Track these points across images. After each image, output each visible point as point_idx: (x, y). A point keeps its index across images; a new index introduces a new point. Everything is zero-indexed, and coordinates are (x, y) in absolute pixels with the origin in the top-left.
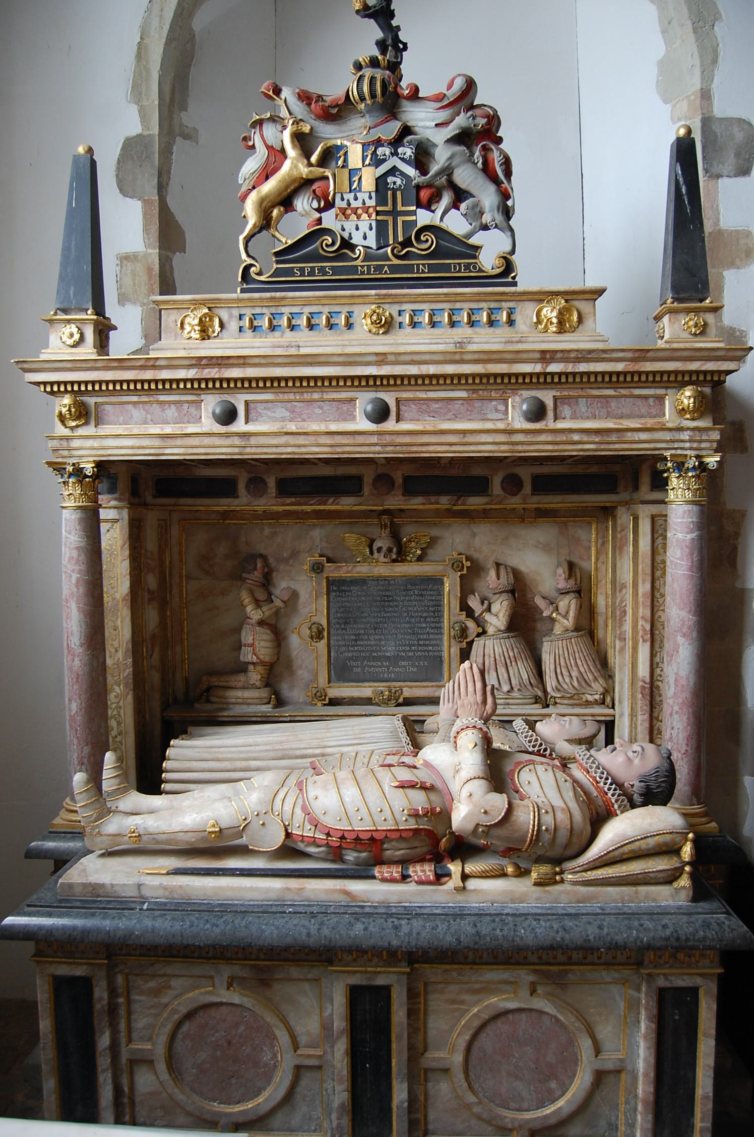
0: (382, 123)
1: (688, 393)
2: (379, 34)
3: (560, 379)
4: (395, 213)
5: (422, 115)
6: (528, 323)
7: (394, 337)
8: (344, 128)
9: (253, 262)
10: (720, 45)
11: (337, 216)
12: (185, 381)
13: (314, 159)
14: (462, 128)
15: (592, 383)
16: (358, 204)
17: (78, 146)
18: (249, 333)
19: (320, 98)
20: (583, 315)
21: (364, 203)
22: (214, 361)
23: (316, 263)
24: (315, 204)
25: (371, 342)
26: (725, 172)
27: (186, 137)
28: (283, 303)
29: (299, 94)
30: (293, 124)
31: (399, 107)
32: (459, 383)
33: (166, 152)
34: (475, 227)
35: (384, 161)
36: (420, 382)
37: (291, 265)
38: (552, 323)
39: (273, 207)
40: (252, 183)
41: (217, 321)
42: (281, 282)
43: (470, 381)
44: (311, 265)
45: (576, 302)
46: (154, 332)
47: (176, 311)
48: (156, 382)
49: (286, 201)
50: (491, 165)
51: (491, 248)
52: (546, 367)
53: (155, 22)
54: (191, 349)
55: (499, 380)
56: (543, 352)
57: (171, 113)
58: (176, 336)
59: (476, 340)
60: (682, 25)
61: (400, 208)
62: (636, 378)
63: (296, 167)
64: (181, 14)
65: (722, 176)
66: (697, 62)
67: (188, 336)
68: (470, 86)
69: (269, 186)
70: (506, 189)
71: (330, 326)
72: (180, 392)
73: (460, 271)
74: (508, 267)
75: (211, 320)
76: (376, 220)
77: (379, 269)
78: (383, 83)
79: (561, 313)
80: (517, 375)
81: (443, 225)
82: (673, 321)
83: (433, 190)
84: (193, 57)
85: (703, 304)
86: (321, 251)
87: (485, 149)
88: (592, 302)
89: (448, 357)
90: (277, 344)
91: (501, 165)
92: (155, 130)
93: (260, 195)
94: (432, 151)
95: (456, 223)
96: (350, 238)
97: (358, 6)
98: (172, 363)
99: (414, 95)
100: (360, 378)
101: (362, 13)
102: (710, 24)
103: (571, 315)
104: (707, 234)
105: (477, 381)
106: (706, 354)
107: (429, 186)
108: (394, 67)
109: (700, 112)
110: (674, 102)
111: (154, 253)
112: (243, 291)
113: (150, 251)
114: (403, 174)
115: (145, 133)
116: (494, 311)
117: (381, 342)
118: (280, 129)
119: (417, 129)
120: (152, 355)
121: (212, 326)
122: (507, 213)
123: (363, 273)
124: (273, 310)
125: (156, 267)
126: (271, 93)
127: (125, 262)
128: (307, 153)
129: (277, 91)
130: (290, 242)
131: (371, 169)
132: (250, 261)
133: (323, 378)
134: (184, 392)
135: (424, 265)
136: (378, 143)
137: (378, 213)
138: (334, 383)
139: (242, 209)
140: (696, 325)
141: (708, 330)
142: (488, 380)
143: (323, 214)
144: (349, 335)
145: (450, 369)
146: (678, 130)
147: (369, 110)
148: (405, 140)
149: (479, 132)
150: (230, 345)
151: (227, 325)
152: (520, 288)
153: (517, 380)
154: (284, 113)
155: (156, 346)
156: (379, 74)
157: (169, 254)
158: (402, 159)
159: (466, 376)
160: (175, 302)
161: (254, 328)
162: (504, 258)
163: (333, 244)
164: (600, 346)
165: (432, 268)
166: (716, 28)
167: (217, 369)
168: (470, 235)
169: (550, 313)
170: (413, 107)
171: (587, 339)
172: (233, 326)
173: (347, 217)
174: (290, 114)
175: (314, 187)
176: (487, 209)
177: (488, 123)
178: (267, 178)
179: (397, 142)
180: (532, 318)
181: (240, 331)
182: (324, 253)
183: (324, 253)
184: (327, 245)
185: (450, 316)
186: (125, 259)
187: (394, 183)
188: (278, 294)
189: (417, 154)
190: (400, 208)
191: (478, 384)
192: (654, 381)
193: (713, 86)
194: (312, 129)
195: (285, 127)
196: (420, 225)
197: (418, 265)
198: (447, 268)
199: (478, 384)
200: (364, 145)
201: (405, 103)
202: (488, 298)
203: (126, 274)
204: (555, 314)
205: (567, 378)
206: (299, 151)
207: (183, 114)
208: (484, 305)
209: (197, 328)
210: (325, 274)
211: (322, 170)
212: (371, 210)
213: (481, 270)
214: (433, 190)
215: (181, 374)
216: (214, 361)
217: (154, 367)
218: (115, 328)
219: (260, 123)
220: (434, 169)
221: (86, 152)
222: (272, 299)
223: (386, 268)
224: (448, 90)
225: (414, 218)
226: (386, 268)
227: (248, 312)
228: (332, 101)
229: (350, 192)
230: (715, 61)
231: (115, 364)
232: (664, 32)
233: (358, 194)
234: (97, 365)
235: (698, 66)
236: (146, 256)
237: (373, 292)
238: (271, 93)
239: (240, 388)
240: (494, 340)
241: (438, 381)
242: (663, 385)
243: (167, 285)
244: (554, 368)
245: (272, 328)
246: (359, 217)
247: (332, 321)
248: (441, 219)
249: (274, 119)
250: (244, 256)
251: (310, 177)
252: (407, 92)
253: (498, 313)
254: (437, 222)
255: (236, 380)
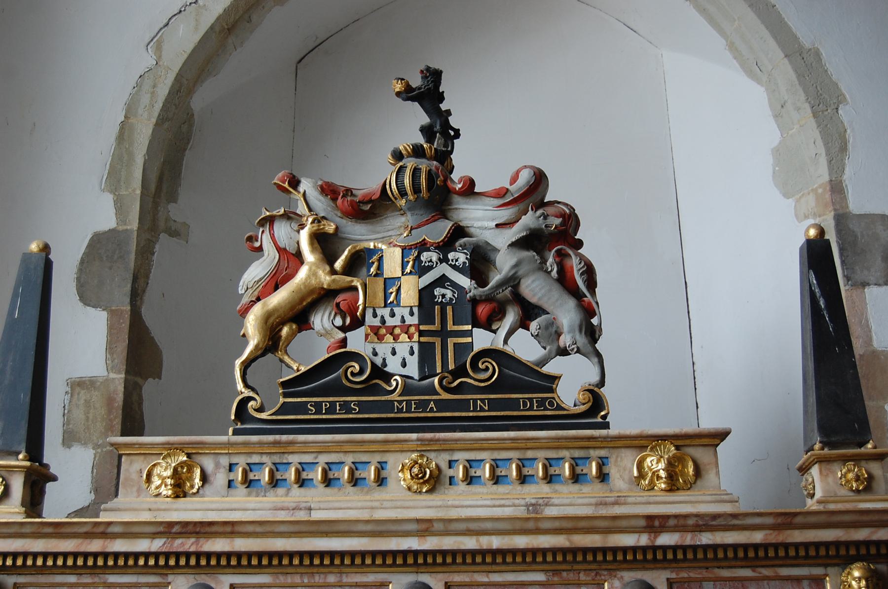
0: (428, 222)
1: (857, 574)
2: (424, 119)
3: (675, 555)
4: (444, 334)
5: (479, 214)
6: (626, 477)
7: (443, 497)
8: (378, 228)
9: (252, 394)
10: (848, 131)
11: (367, 336)
12: (147, 555)
13: (338, 264)
14: (530, 229)
15: (721, 560)
16: (396, 321)
17: (31, 242)
18: (242, 489)
19: (348, 192)
20: (702, 467)
21: (403, 320)
22: (190, 528)
23: (338, 399)
24: (339, 321)
25: (411, 504)
26: (872, 279)
27: (174, 233)
28: (290, 449)
29: (321, 187)
30: (313, 222)
31: (450, 204)
32: (534, 561)
33: (145, 252)
34: (550, 351)
35: (430, 268)
36: (479, 559)
37: (304, 399)
38: (659, 478)
39: (283, 323)
40: (256, 293)
41: (197, 473)
42: (291, 420)
43: (549, 558)
44: (331, 399)
45: (690, 451)
46: (108, 485)
47: (142, 458)
48: (106, 555)
49: (300, 316)
50: (569, 274)
51: (572, 378)
52: (655, 538)
53: (145, 99)
54: (159, 510)
55: (590, 557)
56: (650, 518)
57: (156, 204)
58: (139, 491)
59: (556, 501)
60: (798, 109)
61: (450, 327)
62: (781, 553)
63: (315, 274)
64: (179, 91)
65: (868, 284)
66: (822, 151)
67: (156, 492)
68: (540, 179)
69: (279, 298)
70: (590, 303)
71: (355, 481)
72: (139, 570)
73: (531, 408)
74: (596, 403)
75: (190, 470)
76: (419, 342)
77: (422, 405)
78: (431, 176)
79: (670, 465)
80: (615, 550)
81: (508, 349)
82: (824, 473)
83: (494, 305)
84: (189, 141)
85: (863, 450)
86: (344, 381)
87: (561, 255)
88: (712, 449)
89: (518, 525)
90: (280, 505)
91: (582, 274)
92: (134, 225)
93: (266, 309)
94: (492, 256)
95: (525, 347)
96: (385, 364)
97: (399, 87)
98: (130, 531)
99: (469, 189)
100: (394, 554)
101: (404, 95)
102: (833, 107)
103: (685, 466)
104: (857, 357)
105: (559, 558)
106: (876, 517)
107: (488, 299)
108: (444, 157)
109: (831, 208)
110: (797, 196)
111: (119, 378)
112: (236, 432)
113: (112, 375)
114: (454, 285)
115: (121, 228)
116: (579, 462)
117: (424, 503)
118: (296, 228)
119: (472, 230)
120: (104, 518)
121: (191, 479)
122: (592, 334)
123: (400, 411)
124: (277, 459)
125: (120, 397)
126: (286, 185)
127: (78, 389)
128: (329, 258)
129: (295, 183)
130: (303, 369)
131: (413, 278)
132: (247, 393)
133: (342, 554)
134: (145, 571)
135: (482, 400)
136: (423, 246)
137: (421, 333)
138: (358, 561)
139: (242, 325)
140: (857, 479)
141: (875, 485)
142: (575, 557)
143: (348, 334)
144: (380, 495)
145: (521, 542)
146: (807, 230)
147: (412, 207)
148: (457, 244)
149: (552, 234)
150: (213, 506)
151: (212, 479)
152: (613, 431)
153: (615, 556)
154: (302, 209)
155: (109, 505)
156: (424, 165)
157: (139, 380)
158: (454, 267)
159: (544, 551)
160: (141, 445)
161: (248, 482)
162: (590, 391)
163: (361, 372)
164: (727, 508)
165: (494, 405)
166: (840, 112)
167: (193, 540)
168: (543, 362)
169: (656, 464)
170: (466, 203)
171: (709, 498)
172: (220, 479)
173: (380, 338)
174: (310, 210)
175: (338, 300)
176: (566, 328)
177: (563, 223)
178: (276, 288)
179: (446, 246)
180: (631, 471)
181: (229, 486)
182: (348, 384)
183: (348, 384)
184: (353, 374)
185: (519, 469)
186: (77, 385)
187: (443, 296)
188: (284, 438)
189: (472, 260)
190: (450, 327)
191: (560, 563)
192: (807, 556)
193: (845, 177)
194: (337, 228)
195: (302, 226)
196: (477, 348)
197: (475, 401)
198: (513, 404)
199: (560, 563)
200: (404, 249)
201: (456, 199)
202: (570, 444)
203: (77, 406)
204: (662, 465)
205: (685, 554)
206: (319, 256)
207: (172, 207)
208: (566, 453)
209: (169, 481)
210: (349, 411)
211: (349, 279)
212: (412, 330)
213: (559, 407)
214: (494, 305)
215: (143, 545)
216: (190, 528)
217: (104, 535)
218: (54, 479)
219: (270, 221)
220: (495, 279)
221: (42, 250)
222: (276, 443)
223: (432, 405)
224: (511, 184)
225: (469, 340)
226: (432, 405)
227: (242, 461)
228: (365, 196)
229: (385, 306)
230: (844, 148)
231: (49, 530)
232: (777, 116)
233: (396, 310)
234: (23, 530)
235: (824, 154)
236: (107, 381)
237: (414, 436)
238: (286, 185)
239: (224, 567)
240: (580, 501)
241: (504, 559)
242: (820, 561)
243: (132, 422)
244: (666, 539)
245: (274, 483)
246: (396, 338)
247: (357, 474)
248: (506, 342)
249: (288, 216)
250: (240, 386)
251: (333, 287)
252: (460, 186)
253: (584, 465)
254: (500, 345)
255: (219, 555)
